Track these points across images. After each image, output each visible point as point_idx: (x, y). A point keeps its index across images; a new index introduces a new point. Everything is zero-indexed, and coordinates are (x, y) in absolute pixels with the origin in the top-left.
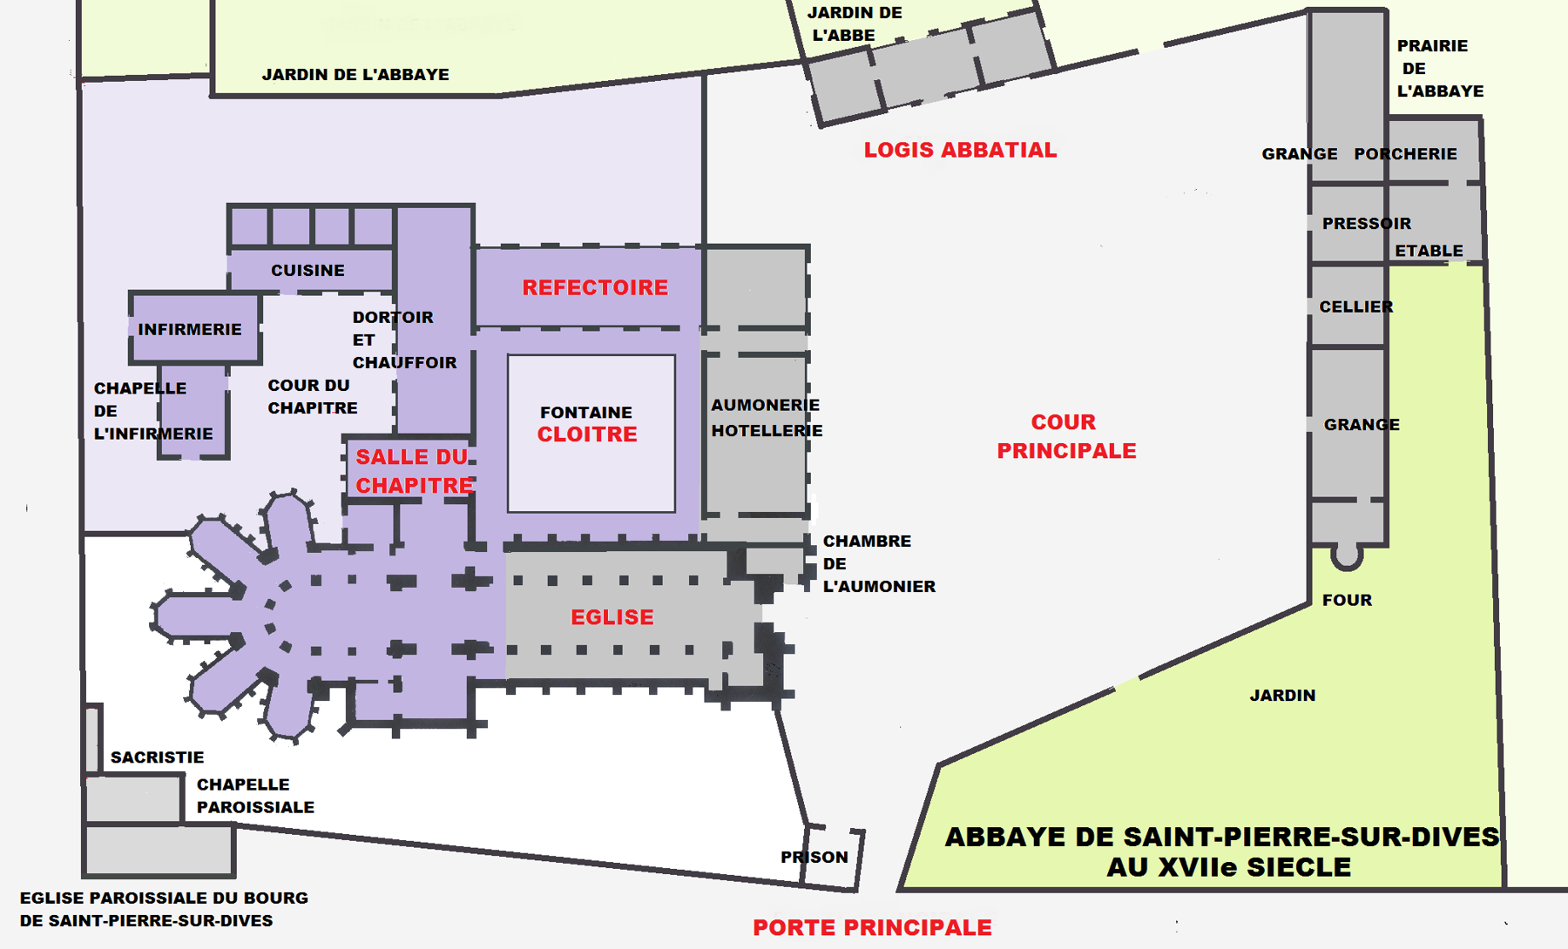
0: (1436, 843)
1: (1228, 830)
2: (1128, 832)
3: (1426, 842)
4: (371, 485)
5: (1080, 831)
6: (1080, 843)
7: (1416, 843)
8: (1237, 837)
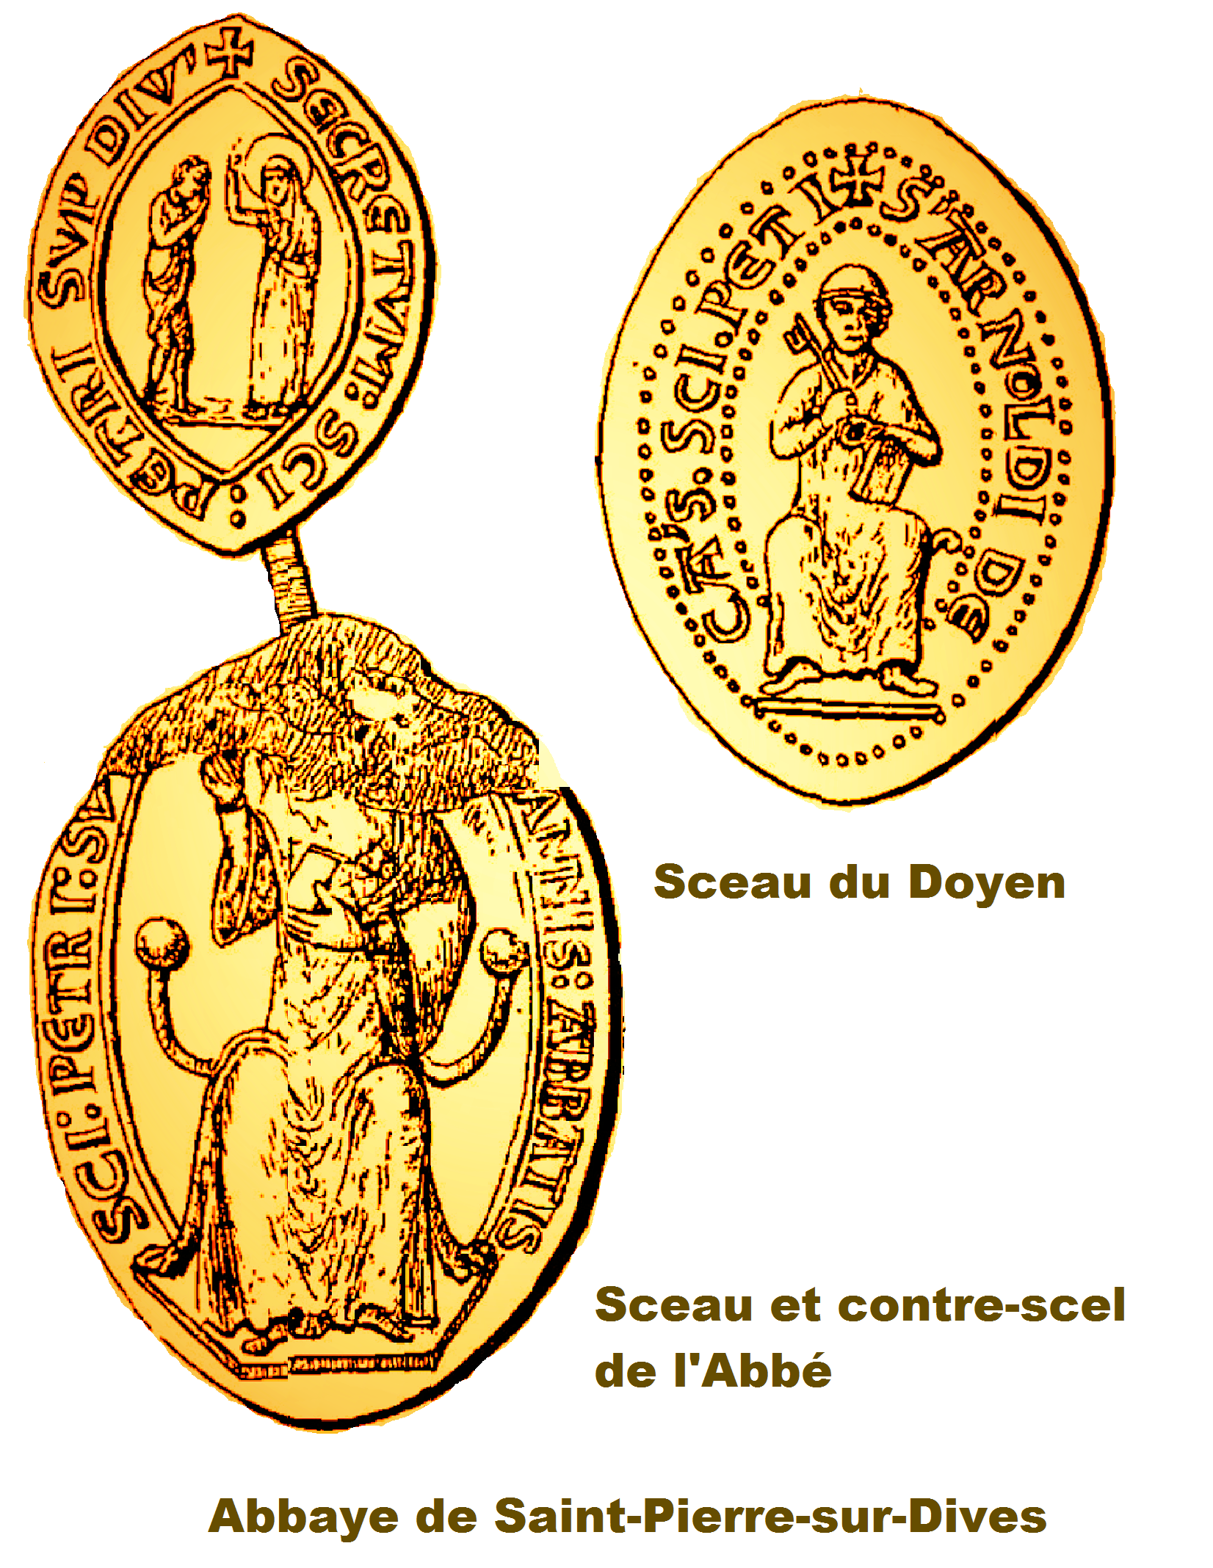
0: (951, 1527)
1: (651, 1504)
2: (501, 1507)
3: (933, 1525)
4: (75, 1103)
5: (916, 870)
6: (916, 892)
7: (917, 1526)
8: (667, 1516)
